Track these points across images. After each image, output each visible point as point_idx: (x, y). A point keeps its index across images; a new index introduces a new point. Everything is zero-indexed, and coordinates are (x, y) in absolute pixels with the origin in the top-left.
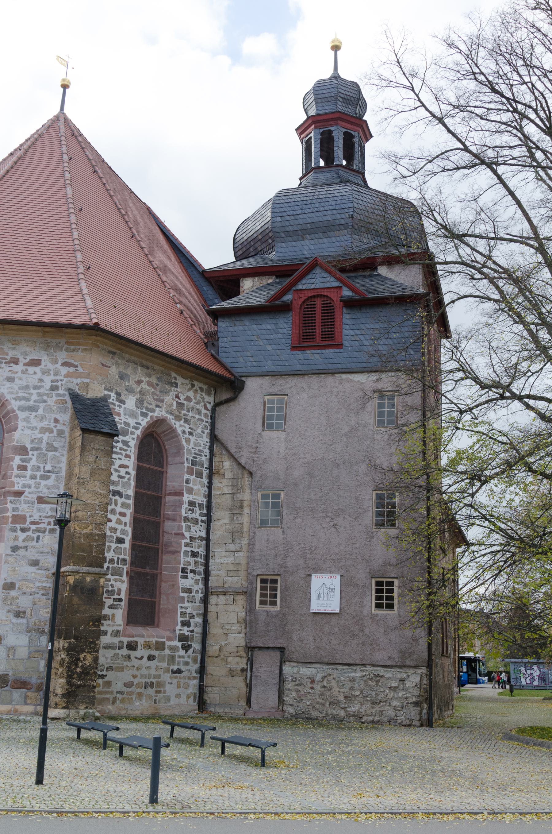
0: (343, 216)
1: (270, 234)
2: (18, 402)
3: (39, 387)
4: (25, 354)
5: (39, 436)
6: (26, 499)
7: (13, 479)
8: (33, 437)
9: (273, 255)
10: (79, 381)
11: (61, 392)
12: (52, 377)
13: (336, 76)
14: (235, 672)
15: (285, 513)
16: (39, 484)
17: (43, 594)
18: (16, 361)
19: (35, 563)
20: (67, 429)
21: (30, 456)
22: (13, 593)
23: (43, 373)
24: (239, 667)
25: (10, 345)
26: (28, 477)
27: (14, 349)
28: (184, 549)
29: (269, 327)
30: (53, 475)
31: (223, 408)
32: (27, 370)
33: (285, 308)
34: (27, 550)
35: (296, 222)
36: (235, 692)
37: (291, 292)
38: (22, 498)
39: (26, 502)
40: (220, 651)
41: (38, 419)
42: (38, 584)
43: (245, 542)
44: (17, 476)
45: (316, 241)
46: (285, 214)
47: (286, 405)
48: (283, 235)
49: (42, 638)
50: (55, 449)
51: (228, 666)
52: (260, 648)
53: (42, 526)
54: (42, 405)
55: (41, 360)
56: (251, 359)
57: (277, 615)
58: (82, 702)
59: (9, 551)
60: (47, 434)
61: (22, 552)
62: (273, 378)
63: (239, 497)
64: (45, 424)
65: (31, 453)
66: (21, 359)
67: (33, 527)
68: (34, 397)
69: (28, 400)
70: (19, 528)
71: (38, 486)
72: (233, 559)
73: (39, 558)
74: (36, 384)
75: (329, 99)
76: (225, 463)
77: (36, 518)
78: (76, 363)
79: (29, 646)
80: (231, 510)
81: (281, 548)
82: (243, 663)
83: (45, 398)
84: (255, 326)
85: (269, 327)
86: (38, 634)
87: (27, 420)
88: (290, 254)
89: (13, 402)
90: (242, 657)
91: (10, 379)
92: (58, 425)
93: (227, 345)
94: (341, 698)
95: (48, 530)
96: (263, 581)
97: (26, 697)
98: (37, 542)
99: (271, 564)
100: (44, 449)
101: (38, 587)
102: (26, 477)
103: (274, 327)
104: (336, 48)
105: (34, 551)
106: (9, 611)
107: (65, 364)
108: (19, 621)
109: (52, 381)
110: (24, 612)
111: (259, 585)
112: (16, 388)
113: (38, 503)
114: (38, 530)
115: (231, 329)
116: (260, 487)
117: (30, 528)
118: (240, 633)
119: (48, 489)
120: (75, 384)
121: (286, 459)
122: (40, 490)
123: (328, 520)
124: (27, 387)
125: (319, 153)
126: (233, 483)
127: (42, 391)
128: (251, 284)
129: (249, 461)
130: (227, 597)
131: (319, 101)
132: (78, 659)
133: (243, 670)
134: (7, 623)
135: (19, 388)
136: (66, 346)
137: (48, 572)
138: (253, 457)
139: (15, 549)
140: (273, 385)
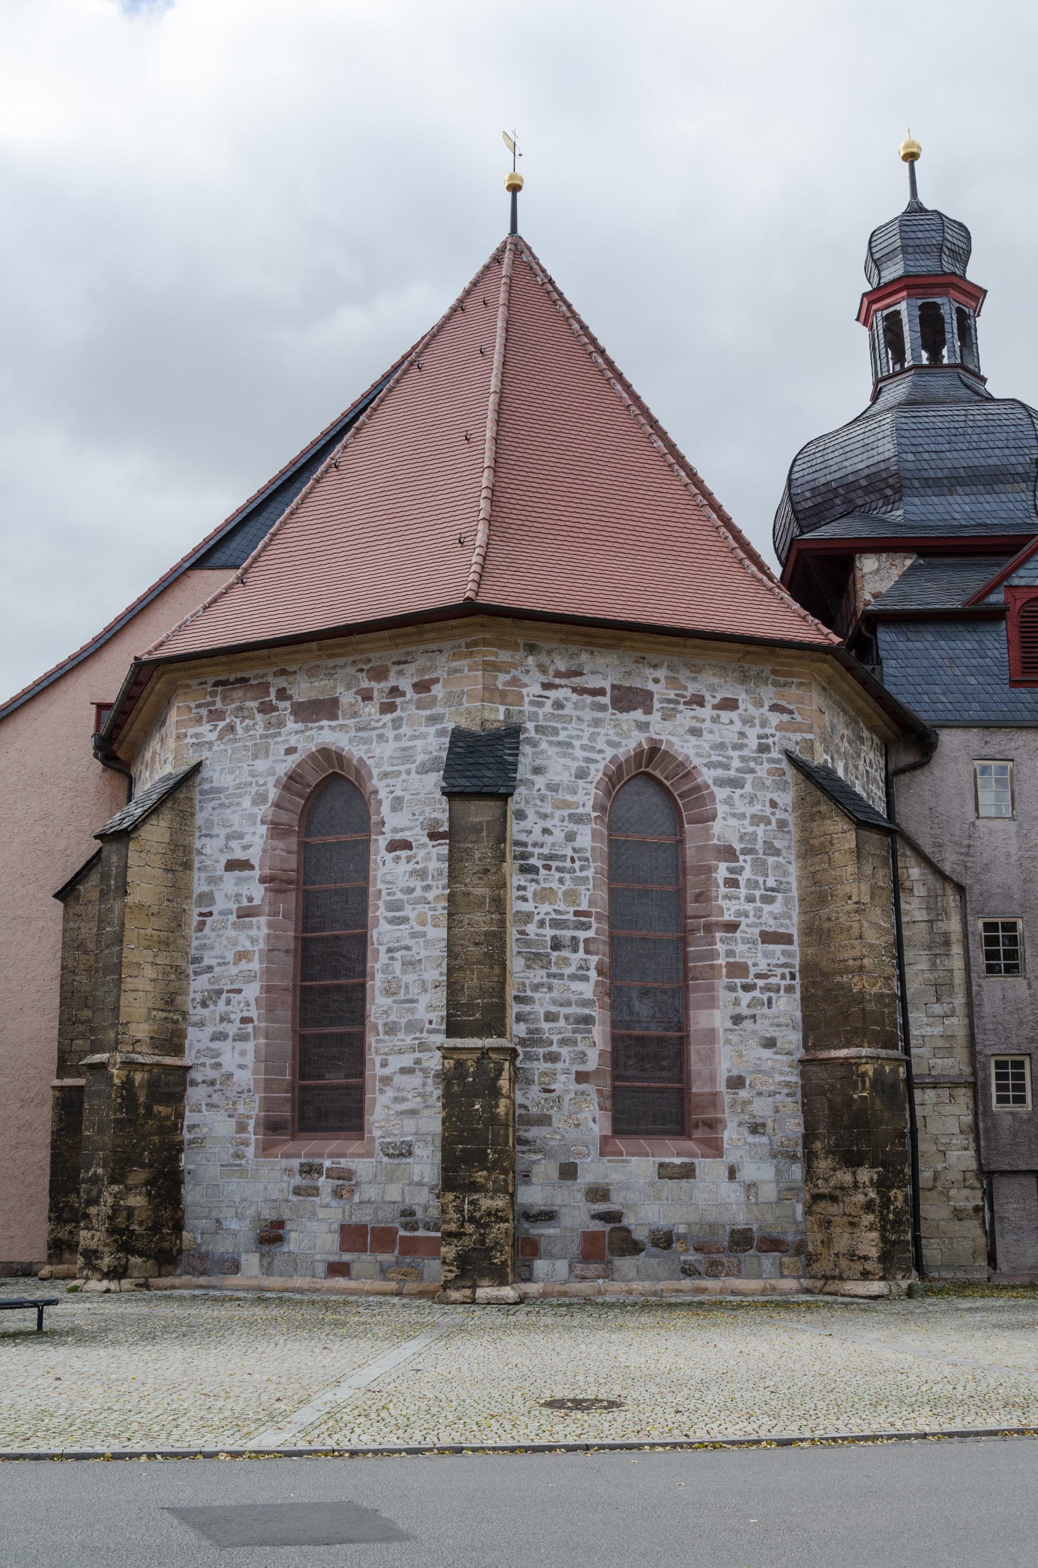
1: (891, 481)
2: (712, 770)
4: (712, 689)
5: (751, 829)
6: (744, 935)
7: (720, 902)
8: (743, 831)
9: (898, 515)
11: (775, 754)
13: (916, 208)
14: (964, 1214)
15: (1028, 954)
16: (760, 910)
17: (787, 1095)
18: (700, 701)
19: (770, 1043)
20: (790, 818)
21: (741, 863)
22: (743, 1094)
23: (745, 722)
24: (970, 1205)
26: (743, 899)
27: (695, 679)
29: (968, 645)
30: (780, 896)
31: (904, 779)
32: (719, 717)
33: (996, 615)
34: (755, 1022)
35: (941, 464)
36: (968, 1245)
37: (1002, 588)
38: (738, 934)
39: (746, 941)
40: (935, 1179)
41: (746, 801)
42: (778, 1078)
43: (960, 1000)
44: (726, 897)
45: (972, 497)
46: (920, 449)
47: (1012, 776)
48: (916, 484)
49: (794, 1167)
50: (777, 853)
51: (952, 1203)
55: (737, 700)
56: (943, 698)
57: (1030, 1119)
58: (899, 1268)
59: (729, 1024)
60: (762, 825)
61: (747, 1024)
62: (986, 732)
65: (741, 857)
66: (708, 697)
67: (761, 983)
68: (736, 763)
69: (727, 767)
70: (739, 985)
72: (941, 1029)
73: (774, 1034)
74: (736, 741)
75: (928, 249)
76: (911, 871)
77: (763, 967)
78: (791, 707)
79: (777, 1182)
80: (930, 948)
81: (1027, 1011)
82: (976, 1198)
83: (752, 764)
84: (942, 643)
85: (968, 645)
86: (788, 1161)
87: (729, 801)
88: (931, 517)
89: (704, 770)
90: (973, 1188)
91: (696, 732)
92: (777, 811)
93: (895, 672)
95: (782, 988)
96: (999, 1065)
97: (781, 1264)
98: (769, 1008)
99: (1014, 1037)
100: (761, 851)
101: (779, 1083)
102: (738, 898)
103: (977, 646)
104: (911, 157)
105: (767, 1022)
106: (740, 1124)
107: (774, 708)
108: (757, 1140)
109: (759, 737)
110: (763, 1125)
111: (993, 1071)
112: (707, 746)
113: (763, 942)
114: (768, 988)
115: (901, 645)
116: (982, 912)
117: (755, 985)
118: (966, 1149)
119: (775, 918)
120: (793, 740)
121: (1021, 865)
122: (763, 920)
124: (722, 746)
125: (919, 342)
126: (928, 903)
127: (745, 752)
128: (876, 566)
129: (958, 869)
130: (939, 1091)
131: (910, 250)
132: (889, 1199)
133: (977, 1209)
134: (740, 1144)
135: (711, 748)
136: (773, 677)
137: (791, 1058)
138: (964, 862)
139: (737, 1019)
140: (986, 742)
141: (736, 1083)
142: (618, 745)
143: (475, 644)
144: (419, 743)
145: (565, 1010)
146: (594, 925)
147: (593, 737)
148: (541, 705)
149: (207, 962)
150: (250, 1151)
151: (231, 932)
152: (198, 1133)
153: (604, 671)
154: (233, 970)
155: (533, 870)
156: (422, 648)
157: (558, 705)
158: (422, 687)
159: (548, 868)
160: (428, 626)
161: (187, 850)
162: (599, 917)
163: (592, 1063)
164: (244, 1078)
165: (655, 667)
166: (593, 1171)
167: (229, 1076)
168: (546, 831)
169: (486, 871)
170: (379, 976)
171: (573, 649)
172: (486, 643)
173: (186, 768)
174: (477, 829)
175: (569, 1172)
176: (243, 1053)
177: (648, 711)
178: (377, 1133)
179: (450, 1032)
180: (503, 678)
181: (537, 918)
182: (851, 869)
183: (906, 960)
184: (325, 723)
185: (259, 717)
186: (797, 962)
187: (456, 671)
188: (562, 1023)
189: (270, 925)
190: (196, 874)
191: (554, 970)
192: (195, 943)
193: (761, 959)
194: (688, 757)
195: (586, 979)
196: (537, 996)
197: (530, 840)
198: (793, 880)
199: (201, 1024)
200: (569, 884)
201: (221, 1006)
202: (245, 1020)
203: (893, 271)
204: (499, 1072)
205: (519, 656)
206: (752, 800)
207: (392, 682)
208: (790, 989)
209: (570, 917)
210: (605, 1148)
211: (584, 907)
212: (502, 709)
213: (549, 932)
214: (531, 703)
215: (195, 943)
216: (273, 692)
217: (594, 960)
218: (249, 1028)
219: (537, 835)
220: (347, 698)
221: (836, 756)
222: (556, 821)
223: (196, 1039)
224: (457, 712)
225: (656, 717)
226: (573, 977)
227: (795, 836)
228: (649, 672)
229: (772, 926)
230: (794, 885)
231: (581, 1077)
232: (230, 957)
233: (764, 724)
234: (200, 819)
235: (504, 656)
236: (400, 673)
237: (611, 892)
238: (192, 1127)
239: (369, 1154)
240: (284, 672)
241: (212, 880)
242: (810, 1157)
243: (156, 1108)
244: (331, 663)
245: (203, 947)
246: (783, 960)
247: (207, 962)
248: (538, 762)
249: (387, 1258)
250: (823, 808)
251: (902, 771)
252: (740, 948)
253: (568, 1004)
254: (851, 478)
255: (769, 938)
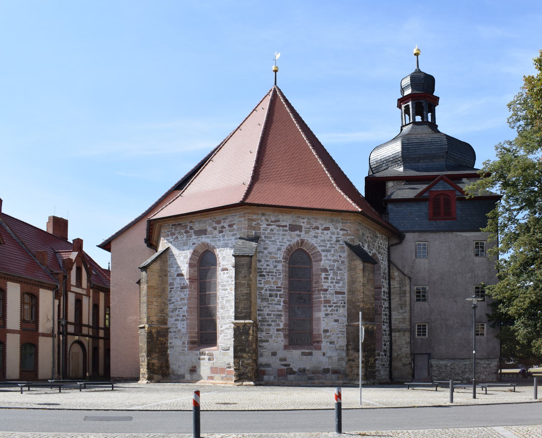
0: (442, 151)
3: (331, 241)
4: (322, 225)
5: (333, 264)
7: (322, 283)
10: (349, 237)
12: (336, 236)
18: (317, 228)
19: (336, 321)
20: (346, 260)
23: (332, 234)
24: (408, 362)
25: (313, 220)
27: (316, 222)
28: (383, 312)
29: (416, 209)
30: (341, 282)
31: (394, 247)
33: (425, 200)
38: (328, 292)
42: (339, 330)
43: (408, 309)
44: (324, 282)
50: (341, 270)
52: (418, 354)
53: (338, 304)
54: (333, 249)
61: (330, 316)
63: (403, 289)
64: (335, 258)
66: (320, 227)
67: (334, 305)
68: (329, 245)
69: (326, 246)
71: (334, 286)
77: (335, 301)
83: (334, 246)
85: (416, 209)
87: (326, 256)
89: (318, 247)
91: (316, 237)
94: (460, 372)
96: (418, 326)
107: (341, 229)
115: (395, 209)
120: (348, 238)
123: (451, 299)
124: (324, 241)
127: (332, 242)
132: (369, 361)
133: (410, 363)
139: (327, 315)
141: (326, 331)
142: (291, 241)
143: (246, 213)
144: (230, 241)
145: (273, 313)
146: (283, 290)
147: (283, 239)
148: (266, 230)
149: (172, 301)
150: (186, 349)
151: (179, 293)
152: (173, 344)
153: (287, 220)
154: (180, 303)
155: (264, 276)
156: (231, 215)
157: (272, 230)
158: (231, 226)
159: (268, 275)
160: (231, 209)
161: (166, 271)
162: (284, 288)
163: (282, 326)
164: (184, 331)
165: (303, 219)
166: (282, 353)
167: (180, 330)
168: (268, 265)
169: (246, 277)
170: (219, 304)
171: (276, 214)
172: (249, 213)
173: (165, 249)
174: (243, 265)
175: (274, 354)
176: (183, 324)
177: (301, 231)
178: (220, 344)
179: (235, 319)
180: (254, 223)
181: (265, 289)
182: (361, 274)
183: (392, 298)
184: (203, 236)
185: (185, 234)
186: (346, 299)
187: (240, 221)
188: (272, 316)
189: (189, 291)
190: (169, 277)
191: (270, 302)
192: (169, 296)
193: (334, 299)
194: (313, 244)
195: (280, 305)
196: (264, 309)
197: (263, 268)
198: (346, 277)
199: (172, 317)
200: (275, 279)
201: (177, 312)
202: (183, 316)
203: (408, 92)
204: (249, 329)
205: (259, 216)
206: (333, 255)
207: (222, 224)
208: (343, 307)
209: (275, 288)
210: (286, 347)
211: (279, 285)
212: (254, 232)
213: (268, 292)
214: (263, 230)
215: (169, 296)
216: (188, 227)
217: (282, 299)
218: (185, 318)
219: (265, 266)
220: (209, 229)
221: (364, 242)
222: (271, 262)
223: (171, 321)
224: (240, 233)
225: (303, 232)
226: (275, 304)
227: (347, 265)
228: (301, 220)
229: (338, 290)
230: (346, 278)
231: (278, 330)
232: (179, 299)
233: (338, 234)
234: (169, 262)
235: (255, 217)
236: (224, 222)
237: (289, 281)
238: (170, 343)
239: (218, 350)
240: (191, 222)
241: (173, 279)
242: (348, 350)
243: (159, 338)
244: (205, 219)
245: (171, 297)
246: (341, 299)
247: (172, 301)
248: (265, 246)
249: (224, 375)
250: (354, 257)
251: (393, 245)
252: (328, 296)
253: (274, 311)
254: (388, 158)
255: (337, 293)
